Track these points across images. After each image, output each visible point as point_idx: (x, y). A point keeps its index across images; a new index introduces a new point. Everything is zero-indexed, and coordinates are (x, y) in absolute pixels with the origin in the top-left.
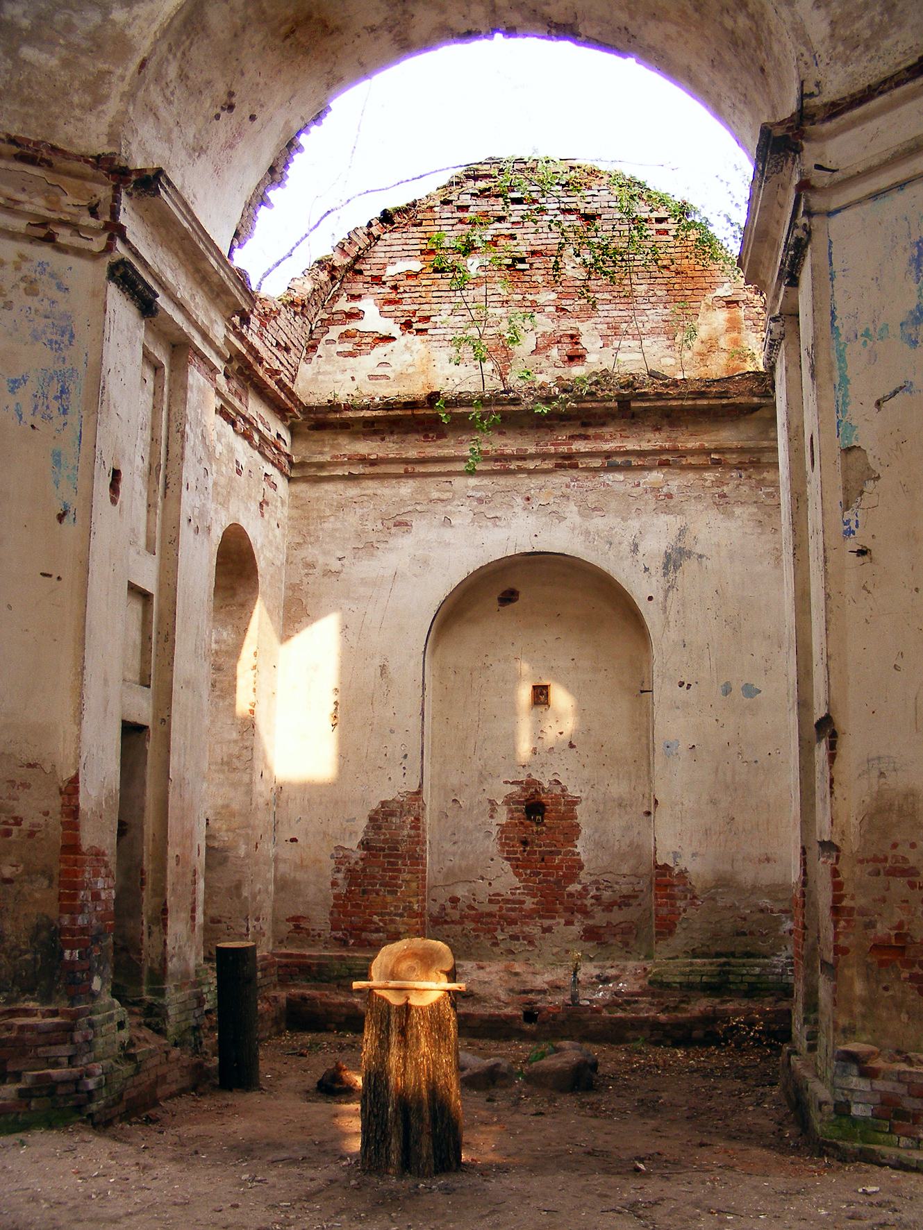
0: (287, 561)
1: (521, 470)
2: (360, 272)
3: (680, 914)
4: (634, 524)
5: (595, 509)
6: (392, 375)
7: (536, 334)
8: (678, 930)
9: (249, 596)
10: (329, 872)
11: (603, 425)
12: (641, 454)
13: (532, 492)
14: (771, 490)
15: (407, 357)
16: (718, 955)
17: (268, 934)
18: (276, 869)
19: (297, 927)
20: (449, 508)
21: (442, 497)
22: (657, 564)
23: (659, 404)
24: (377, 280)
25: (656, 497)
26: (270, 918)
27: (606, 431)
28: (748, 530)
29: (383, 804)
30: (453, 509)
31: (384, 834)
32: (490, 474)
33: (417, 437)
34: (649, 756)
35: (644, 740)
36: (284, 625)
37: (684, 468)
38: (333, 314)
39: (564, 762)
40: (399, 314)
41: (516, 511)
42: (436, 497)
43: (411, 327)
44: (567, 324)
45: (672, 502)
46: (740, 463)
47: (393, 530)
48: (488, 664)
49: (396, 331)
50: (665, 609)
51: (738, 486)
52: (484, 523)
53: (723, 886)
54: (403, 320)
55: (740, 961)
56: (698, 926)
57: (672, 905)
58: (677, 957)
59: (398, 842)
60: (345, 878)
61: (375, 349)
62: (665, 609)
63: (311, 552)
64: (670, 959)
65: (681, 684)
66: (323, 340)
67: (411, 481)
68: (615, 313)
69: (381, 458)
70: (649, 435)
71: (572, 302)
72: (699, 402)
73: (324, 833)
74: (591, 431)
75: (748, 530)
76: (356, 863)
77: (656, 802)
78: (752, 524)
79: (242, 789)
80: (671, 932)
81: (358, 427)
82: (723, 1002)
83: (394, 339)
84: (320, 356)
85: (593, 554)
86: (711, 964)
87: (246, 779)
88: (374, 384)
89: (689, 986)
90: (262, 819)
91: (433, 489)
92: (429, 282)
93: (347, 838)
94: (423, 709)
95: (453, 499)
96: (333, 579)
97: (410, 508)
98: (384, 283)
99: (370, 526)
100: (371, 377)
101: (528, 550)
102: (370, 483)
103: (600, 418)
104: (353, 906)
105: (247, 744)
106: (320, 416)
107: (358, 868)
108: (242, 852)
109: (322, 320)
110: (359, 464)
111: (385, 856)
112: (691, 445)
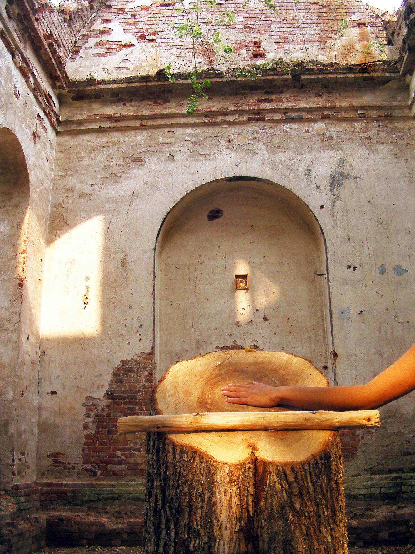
0: (53, 188)
1: (224, 122)
2: (110, 7)
3: (359, 440)
4: (307, 157)
5: (278, 147)
6: (131, 67)
7: (231, 41)
8: (359, 453)
9: (22, 199)
10: (81, 417)
11: (281, 93)
12: (309, 110)
13: (232, 137)
14: (401, 134)
15: (142, 56)
16: (391, 471)
17: (33, 467)
18: (40, 416)
19: (56, 462)
20: (172, 148)
21: (167, 141)
22: (325, 184)
23: (320, 76)
24: (121, 11)
25: (321, 139)
26: (34, 454)
27: (284, 96)
28: (387, 160)
29: (124, 362)
30: (175, 149)
31: (125, 386)
32: (202, 126)
33: (149, 103)
34: (323, 325)
35: (319, 314)
36: (49, 232)
37: (340, 120)
38: (91, 31)
39: (261, 331)
40: (136, 31)
41: (221, 149)
42: (163, 141)
43: (145, 38)
44: (252, 36)
45: (333, 143)
46: (379, 116)
47: (132, 164)
48: (201, 261)
49: (134, 41)
50: (333, 214)
51: (378, 132)
52: (198, 158)
53: (390, 417)
54: (139, 34)
55: (409, 475)
56: (374, 449)
57: (353, 434)
58: (359, 475)
59: (135, 392)
60: (94, 422)
61: (120, 52)
62: (333, 214)
63: (71, 181)
64: (353, 476)
65: (349, 267)
66: (84, 47)
67: (144, 132)
68: (284, 29)
69: (124, 116)
70: (314, 99)
71: (254, 23)
72: (348, 75)
73: (78, 387)
74: (273, 97)
75: (388, 160)
76: (103, 409)
77: (336, 355)
78: (390, 156)
79: (11, 346)
80: (353, 455)
81: (107, 97)
82: (399, 508)
83: (133, 45)
84: (81, 57)
85: (279, 177)
86: (387, 478)
87: (14, 337)
88: (118, 73)
89: (371, 497)
90: (27, 372)
91: (161, 136)
92: (157, 12)
93: (95, 390)
94: (154, 291)
95: (175, 143)
96: (87, 199)
97: (144, 150)
98: (126, 13)
99: (114, 162)
100: (117, 68)
101: (231, 175)
102: (115, 134)
103: (279, 88)
104: (101, 444)
105: (16, 310)
106: (80, 88)
107: (104, 413)
108: (10, 396)
109: (83, 35)
110: (107, 121)
111: (126, 403)
112: (345, 104)
